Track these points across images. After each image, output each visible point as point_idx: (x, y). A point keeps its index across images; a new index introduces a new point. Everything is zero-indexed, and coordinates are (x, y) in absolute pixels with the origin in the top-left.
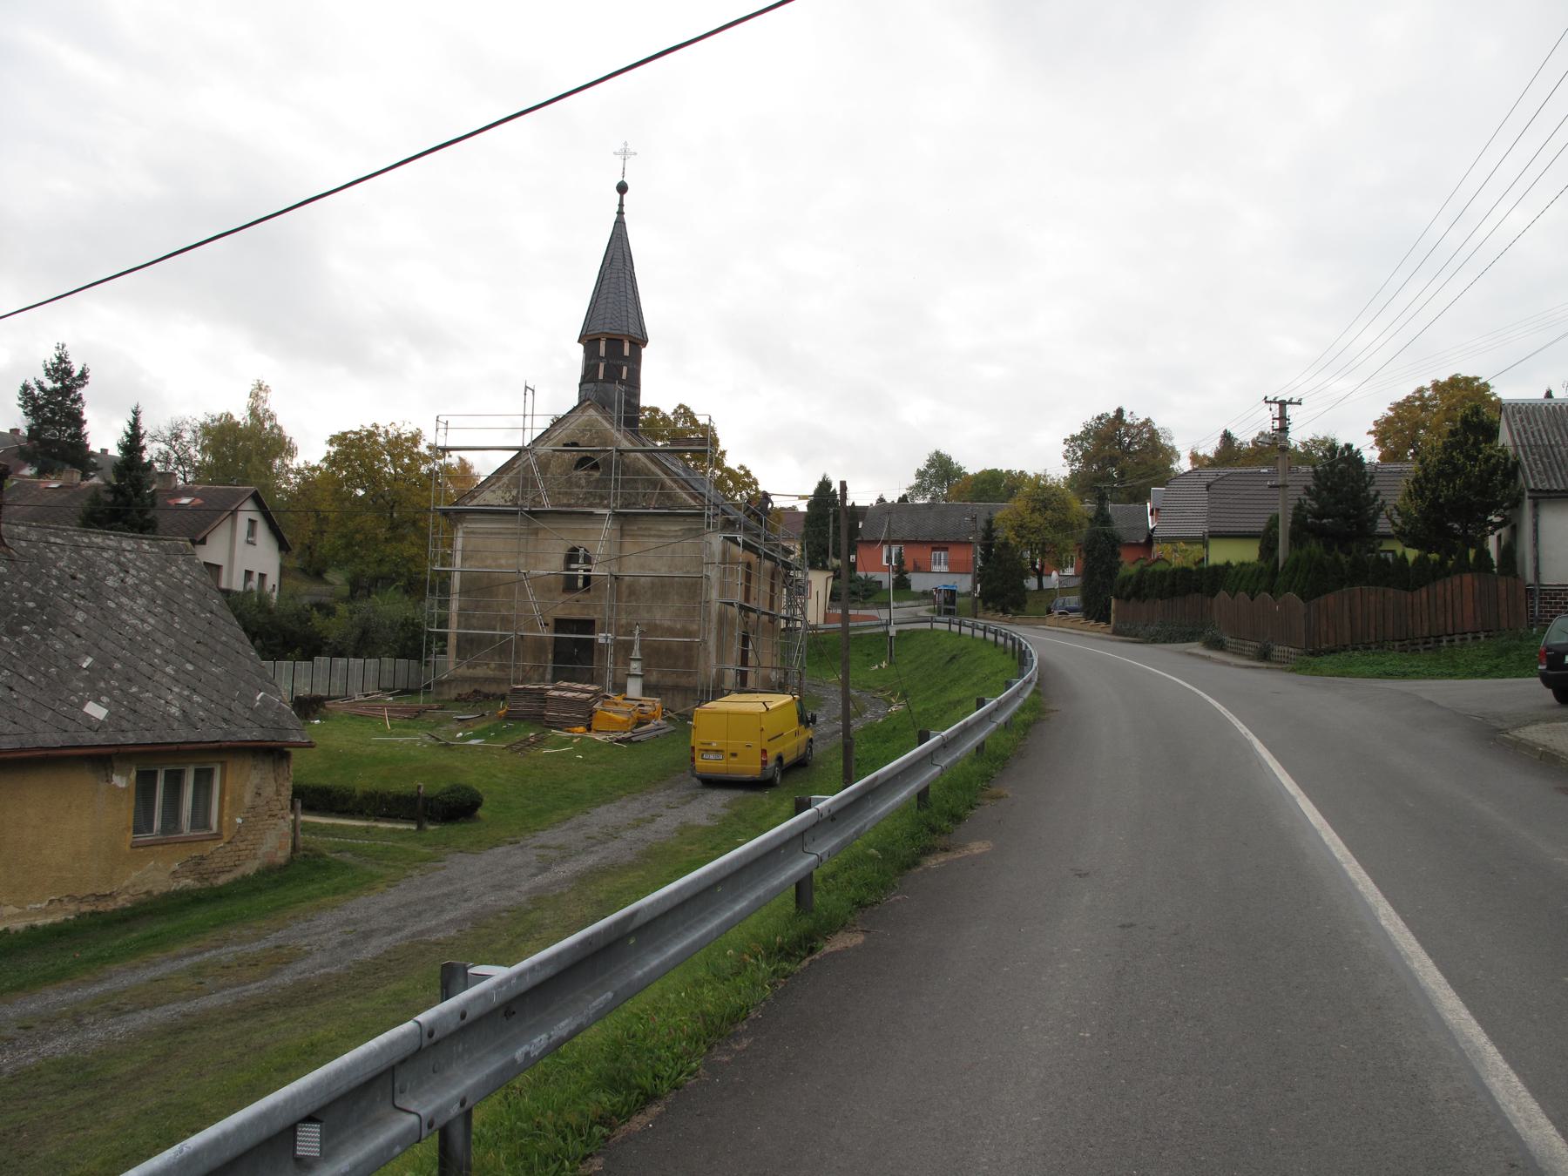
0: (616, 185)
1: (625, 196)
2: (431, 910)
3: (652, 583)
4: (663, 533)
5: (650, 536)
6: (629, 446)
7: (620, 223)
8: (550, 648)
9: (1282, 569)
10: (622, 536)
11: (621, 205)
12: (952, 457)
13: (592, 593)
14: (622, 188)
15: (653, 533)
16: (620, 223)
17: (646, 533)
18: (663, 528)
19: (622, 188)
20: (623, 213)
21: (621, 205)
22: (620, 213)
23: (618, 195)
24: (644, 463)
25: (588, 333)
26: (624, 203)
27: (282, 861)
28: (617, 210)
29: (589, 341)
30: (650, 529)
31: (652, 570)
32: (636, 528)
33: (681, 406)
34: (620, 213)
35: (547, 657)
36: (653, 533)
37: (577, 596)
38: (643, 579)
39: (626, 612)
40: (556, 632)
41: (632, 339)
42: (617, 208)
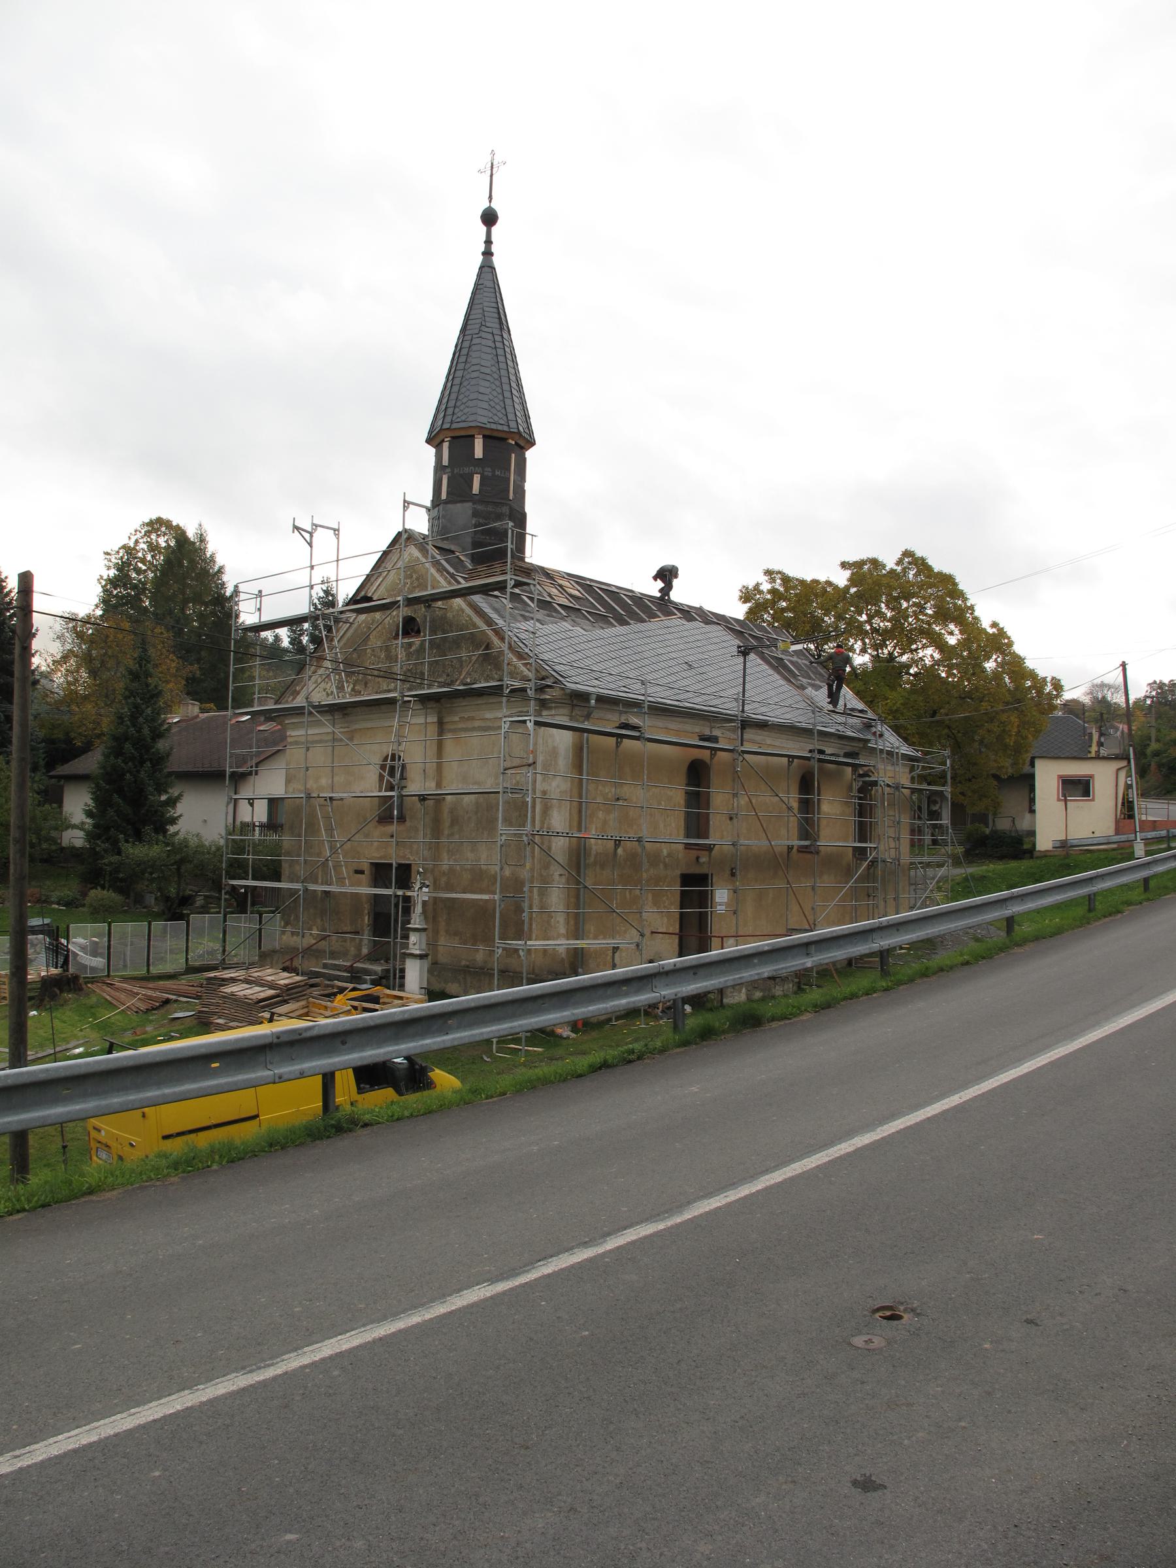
0: (480, 214)
1: (494, 229)
2: (210, 1363)
3: (477, 803)
4: (489, 724)
5: (474, 729)
6: (444, 586)
7: (487, 270)
8: (366, 908)
9: (193, 1011)
10: (441, 732)
11: (488, 242)
12: (227, 569)
13: (408, 823)
14: (489, 218)
15: (477, 724)
16: (487, 270)
17: (469, 725)
18: (488, 716)
19: (489, 218)
20: (492, 254)
21: (488, 242)
22: (488, 254)
23: (484, 228)
24: (469, 616)
25: (454, 426)
26: (493, 239)
27: (757, 998)
28: (483, 249)
29: (453, 438)
30: (472, 719)
31: (475, 783)
32: (457, 719)
33: (907, 554)
34: (488, 254)
35: (363, 920)
36: (477, 724)
37: (393, 828)
38: (466, 798)
39: (449, 851)
40: (376, 885)
41: (487, 433)
42: (482, 248)
